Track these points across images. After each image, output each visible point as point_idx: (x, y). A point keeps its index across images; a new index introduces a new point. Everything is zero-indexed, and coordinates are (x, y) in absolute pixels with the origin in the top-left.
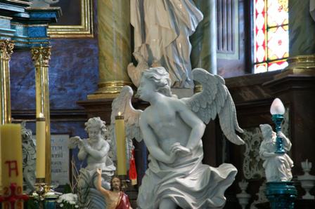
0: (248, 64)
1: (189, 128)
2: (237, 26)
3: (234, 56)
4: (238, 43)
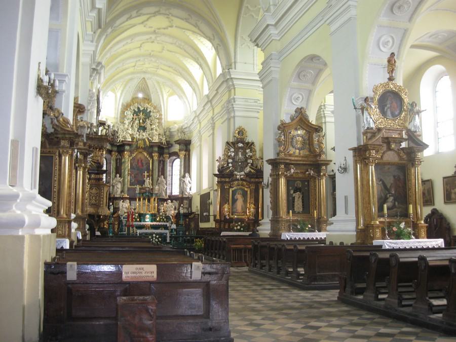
0: (172, 193)
1: (172, 207)
2: (171, 187)
3: (170, 192)
4: (170, 189)
